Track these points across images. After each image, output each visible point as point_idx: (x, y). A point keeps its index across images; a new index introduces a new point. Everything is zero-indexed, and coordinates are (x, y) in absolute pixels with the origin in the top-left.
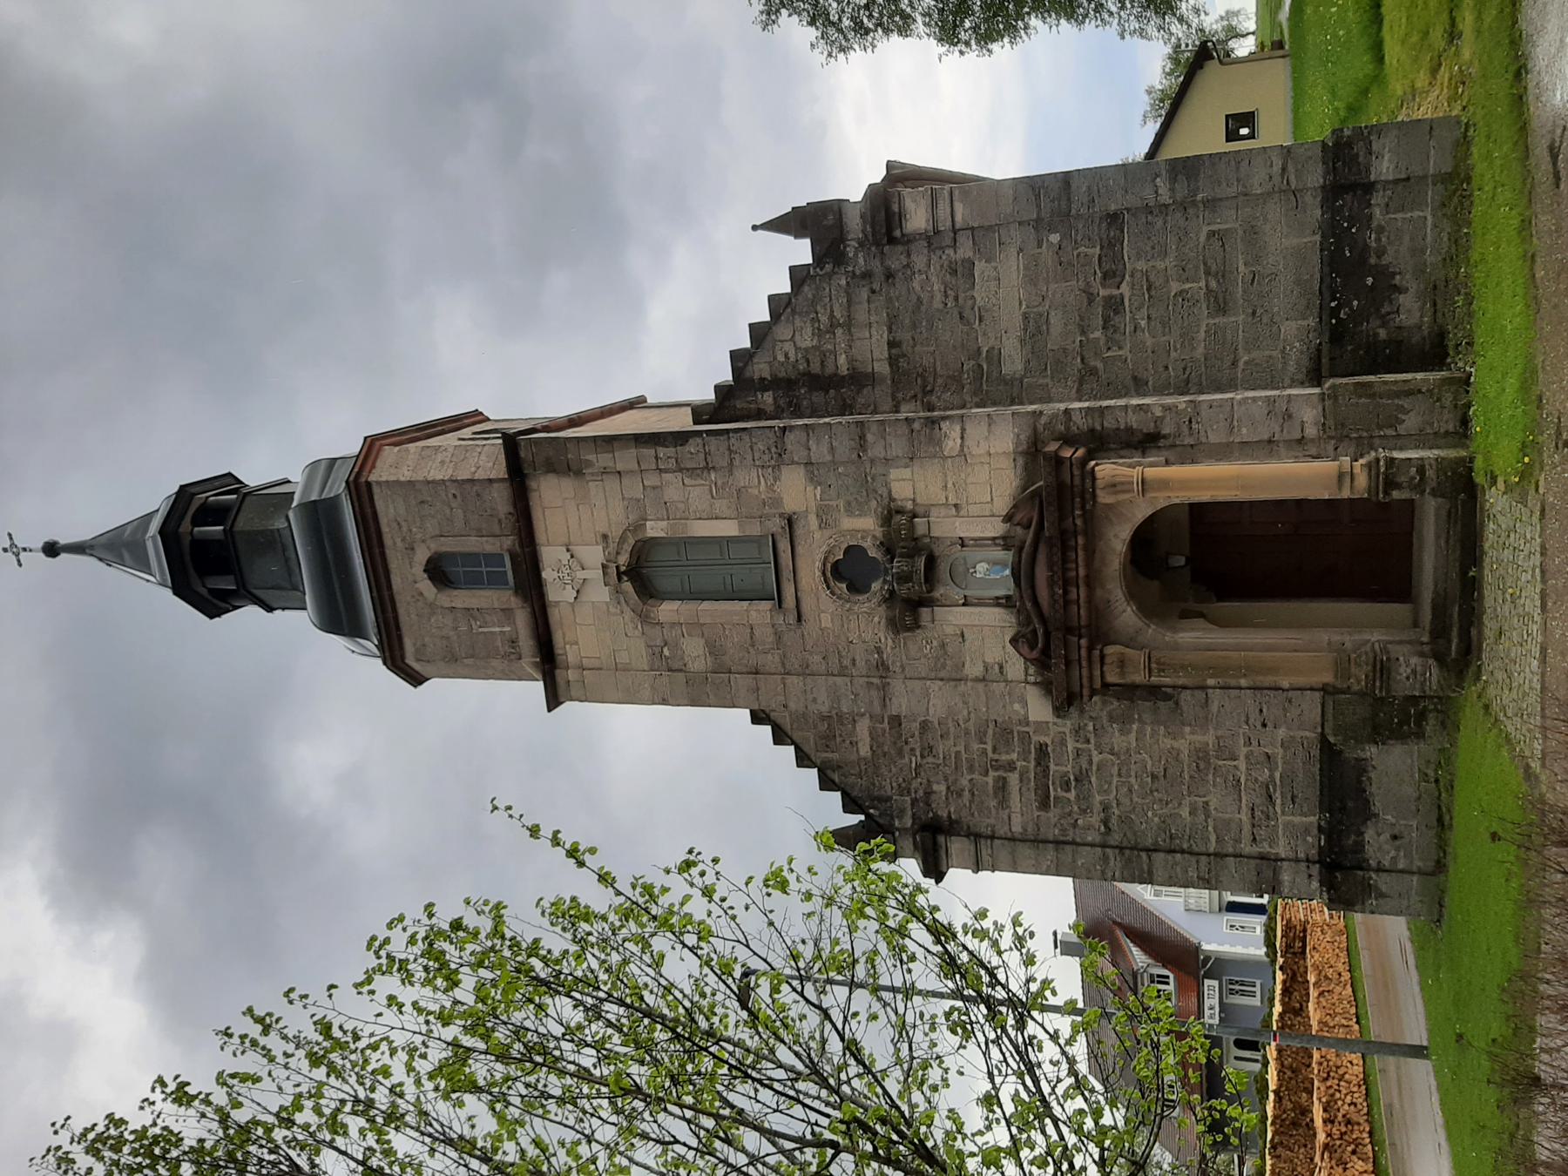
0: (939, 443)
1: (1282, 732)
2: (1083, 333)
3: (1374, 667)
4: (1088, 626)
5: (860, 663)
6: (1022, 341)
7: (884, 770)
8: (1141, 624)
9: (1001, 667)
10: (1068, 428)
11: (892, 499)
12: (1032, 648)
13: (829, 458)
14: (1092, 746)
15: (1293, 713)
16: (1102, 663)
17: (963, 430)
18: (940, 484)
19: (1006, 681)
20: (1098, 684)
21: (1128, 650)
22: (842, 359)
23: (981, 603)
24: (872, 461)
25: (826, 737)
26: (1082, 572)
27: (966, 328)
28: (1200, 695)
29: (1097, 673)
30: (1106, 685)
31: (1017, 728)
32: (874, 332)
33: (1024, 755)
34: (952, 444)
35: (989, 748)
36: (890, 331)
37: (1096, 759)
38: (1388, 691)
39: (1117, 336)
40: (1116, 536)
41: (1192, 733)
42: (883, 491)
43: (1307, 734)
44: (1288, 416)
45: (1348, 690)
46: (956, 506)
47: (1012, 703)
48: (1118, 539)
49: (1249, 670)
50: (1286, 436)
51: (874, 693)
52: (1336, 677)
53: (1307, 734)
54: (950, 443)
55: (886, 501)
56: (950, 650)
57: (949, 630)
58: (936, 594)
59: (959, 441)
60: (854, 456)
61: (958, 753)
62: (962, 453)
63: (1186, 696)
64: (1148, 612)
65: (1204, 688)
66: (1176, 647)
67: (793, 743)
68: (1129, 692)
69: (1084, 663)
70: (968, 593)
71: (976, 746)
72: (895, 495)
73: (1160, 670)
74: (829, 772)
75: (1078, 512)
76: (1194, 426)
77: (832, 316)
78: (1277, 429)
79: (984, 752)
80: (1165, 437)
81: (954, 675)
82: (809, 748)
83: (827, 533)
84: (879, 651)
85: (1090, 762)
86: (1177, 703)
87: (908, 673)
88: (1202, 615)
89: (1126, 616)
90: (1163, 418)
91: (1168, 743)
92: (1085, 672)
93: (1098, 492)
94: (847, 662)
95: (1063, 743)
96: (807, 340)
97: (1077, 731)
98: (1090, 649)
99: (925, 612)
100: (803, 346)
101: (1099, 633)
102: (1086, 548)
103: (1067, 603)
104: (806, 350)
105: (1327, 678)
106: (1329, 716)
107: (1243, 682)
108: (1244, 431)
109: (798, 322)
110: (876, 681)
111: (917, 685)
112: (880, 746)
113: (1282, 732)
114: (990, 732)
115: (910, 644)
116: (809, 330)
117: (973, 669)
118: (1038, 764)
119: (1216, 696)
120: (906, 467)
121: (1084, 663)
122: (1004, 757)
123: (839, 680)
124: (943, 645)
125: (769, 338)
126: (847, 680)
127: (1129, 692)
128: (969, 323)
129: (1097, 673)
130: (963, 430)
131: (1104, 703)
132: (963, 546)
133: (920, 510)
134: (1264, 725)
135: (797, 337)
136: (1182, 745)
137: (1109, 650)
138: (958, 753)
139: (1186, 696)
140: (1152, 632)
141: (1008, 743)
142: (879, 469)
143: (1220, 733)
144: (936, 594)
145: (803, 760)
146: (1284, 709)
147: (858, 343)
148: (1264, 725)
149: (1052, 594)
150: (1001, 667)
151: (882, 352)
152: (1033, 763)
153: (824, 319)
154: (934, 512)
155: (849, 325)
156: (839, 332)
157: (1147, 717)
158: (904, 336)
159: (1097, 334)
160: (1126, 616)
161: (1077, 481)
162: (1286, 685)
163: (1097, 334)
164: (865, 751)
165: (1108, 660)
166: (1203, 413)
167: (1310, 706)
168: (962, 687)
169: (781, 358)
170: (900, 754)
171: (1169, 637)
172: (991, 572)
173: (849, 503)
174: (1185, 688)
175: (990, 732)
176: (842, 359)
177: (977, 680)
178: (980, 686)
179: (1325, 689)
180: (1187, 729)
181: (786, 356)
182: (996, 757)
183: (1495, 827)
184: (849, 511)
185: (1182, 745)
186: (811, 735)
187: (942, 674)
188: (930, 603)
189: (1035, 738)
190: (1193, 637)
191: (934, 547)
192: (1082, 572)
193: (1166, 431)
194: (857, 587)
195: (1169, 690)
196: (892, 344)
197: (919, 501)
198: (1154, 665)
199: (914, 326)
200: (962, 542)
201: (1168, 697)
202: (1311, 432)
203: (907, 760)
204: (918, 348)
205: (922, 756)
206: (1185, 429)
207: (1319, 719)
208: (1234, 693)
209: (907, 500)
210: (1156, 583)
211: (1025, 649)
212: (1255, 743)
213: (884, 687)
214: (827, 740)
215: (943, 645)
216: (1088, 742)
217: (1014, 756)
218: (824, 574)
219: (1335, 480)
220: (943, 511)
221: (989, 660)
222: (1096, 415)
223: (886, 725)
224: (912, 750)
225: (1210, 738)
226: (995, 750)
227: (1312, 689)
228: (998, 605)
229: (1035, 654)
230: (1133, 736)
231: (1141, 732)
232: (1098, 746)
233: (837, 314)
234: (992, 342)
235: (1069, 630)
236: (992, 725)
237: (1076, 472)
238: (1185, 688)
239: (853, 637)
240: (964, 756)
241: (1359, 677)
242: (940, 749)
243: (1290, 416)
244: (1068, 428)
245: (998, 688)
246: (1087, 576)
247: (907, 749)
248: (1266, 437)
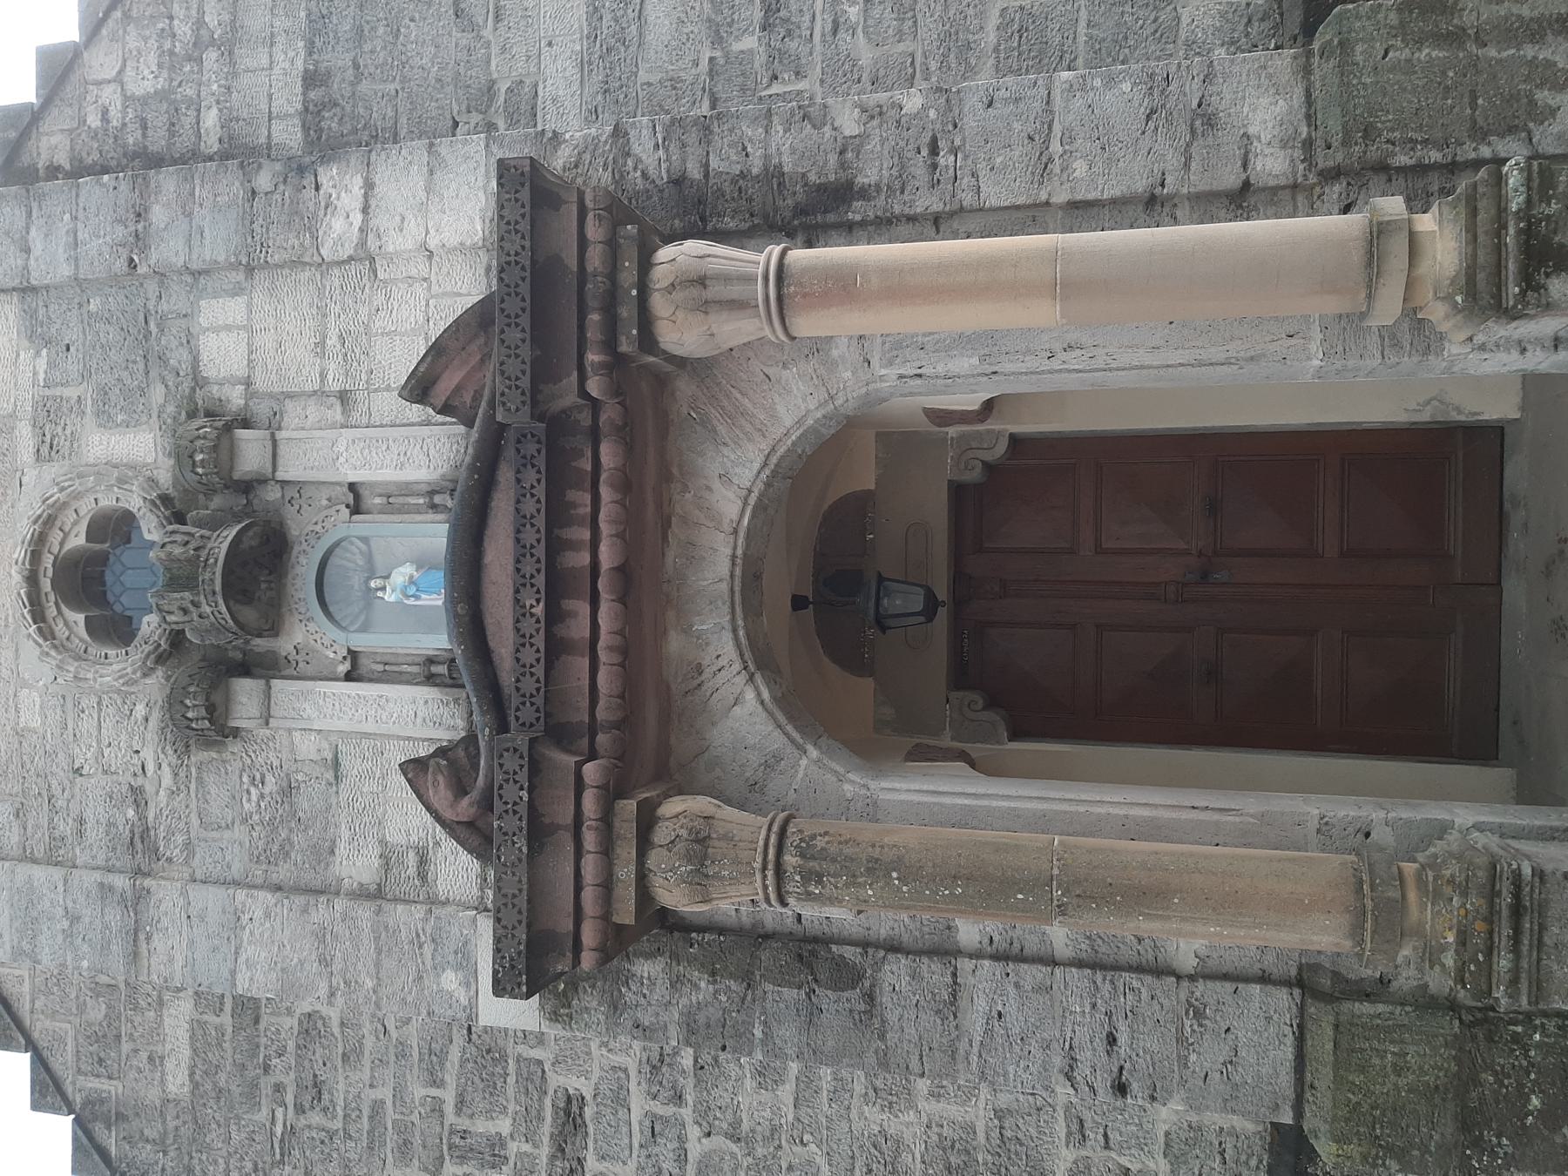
0: (311, 226)
1: (1169, 1114)
2: (718, 40)
3: (1493, 895)
4: (617, 725)
5: (94, 834)
6: (584, 65)
7: (213, 1137)
8: (777, 741)
9: (423, 861)
10: (620, 178)
11: (199, 381)
12: (460, 788)
13: (66, 271)
14: (687, 1113)
15: (1207, 1056)
16: (644, 843)
17: (369, 186)
18: (310, 340)
19: (433, 901)
20: (626, 913)
21: (729, 812)
22: (211, 119)
23: (389, 676)
24: (160, 275)
25: (97, 1038)
26: (607, 556)
27: (465, 39)
28: (934, 973)
29: (625, 873)
30: (667, 922)
31: (515, 1050)
32: (279, 56)
33: (528, 1122)
34: (340, 230)
35: (449, 1096)
36: (310, 49)
37: (695, 1149)
38: (1539, 990)
39: (792, 45)
40: (724, 477)
41: (935, 1095)
42: (179, 358)
43: (1237, 1122)
44: (1205, 119)
45: (1377, 989)
46: (344, 397)
47: (438, 969)
48: (729, 481)
49: (1084, 890)
50: (1199, 181)
51: (114, 916)
52: (1356, 932)
53: (1237, 1122)
54: (338, 225)
55: (186, 386)
56: (303, 803)
57: (308, 747)
58: (284, 646)
59: (357, 219)
60: (120, 265)
61: (377, 1108)
62: (365, 257)
63: (894, 973)
64: (803, 710)
65: (946, 952)
66: (872, 811)
67: (31, 1046)
68: (741, 951)
69: (590, 840)
70: (360, 642)
71: (418, 1091)
72: (209, 371)
73: (810, 876)
74: (99, 1129)
75: (593, 357)
76: (945, 159)
77: (200, 23)
78: (1173, 161)
79: (437, 1109)
80: (864, 194)
81: (308, 877)
82: (63, 1063)
83: (53, 470)
84: (137, 796)
85: (682, 1157)
86: (870, 997)
87: (203, 862)
88: (964, 757)
89: (741, 714)
90: (863, 137)
91: (875, 1117)
92: (590, 866)
93: (660, 305)
94: (65, 827)
95: (620, 1099)
96: (145, 81)
97: (656, 1066)
98: (613, 792)
99: (246, 692)
100: (139, 92)
101: (651, 748)
102: (627, 485)
103: (555, 649)
104: (144, 101)
105: (1324, 937)
106: (1322, 1076)
107: (1060, 936)
108: (1080, 168)
109: (133, 42)
110: (121, 882)
111: (210, 899)
112: (213, 1070)
113: (1169, 1114)
114: (455, 1054)
115: (210, 779)
116: (152, 59)
117: (356, 864)
118: (560, 1150)
119: (981, 978)
120: (237, 291)
121: (590, 840)
122: (481, 1126)
123: (39, 873)
124: (288, 790)
125: (74, 78)
126: (57, 874)
127: (741, 951)
128: (473, 27)
129: (625, 873)
130: (369, 186)
131: (676, 983)
132: (356, 509)
133: (262, 409)
134: (1121, 1089)
135: (129, 72)
136: (907, 1125)
137: (673, 806)
138: (377, 1108)
139: (894, 973)
140: (817, 774)
141: (492, 1088)
142: (176, 300)
143: (1004, 1100)
144: (284, 646)
145: (48, 1091)
146: (1180, 1039)
147: (246, 80)
148: (1121, 1089)
149: (521, 613)
150: (423, 861)
151: (289, 98)
152: (545, 1151)
153: (184, 30)
154: (293, 413)
155: (228, 45)
156: (211, 56)
157: (787, 1033)
158: (338, 59)
159: (749, 42)
160: (741, 714)
161: (596, 258)
162: (1185, 950)
163: (749, 42)
164: (177, 1081)
165: (662, 834)
166: (969, 123)
167: (1260, 1030)
168: (321, 913)
169: (94, 121)
170: (251, 1094)
171: (855, 783)
172: (404, 582)
173: (104, 392)
174: (894, 947)
175: (455, 1054)
176: (211, 119)
177: (363, 894)
178: (364, 913)
179: (1310, 983)
180: (923, 1085)
181: (105, 112)
182: (463, 1123)
183: (1104, 1095)
184: (105, 419)
185: (907, 1125)
186: (66, 1028)
187: (283, 873)
188: (264, 667)
189: (555, 1080)
190: (927, 799)
191: (290, 512)
192: (607, 556)
193: (869, 175)
194: (113, 628)
195: (850, 952)
196: (311, 79)
197: (260, 384)
198: (790, 860)
199: (359, 34)
200: (356, 499)
201: (847, 977)
202: (1272, 165)
203: (263, 1115)
204: (364, 87)
205: (300, 1109)
206: (919, 169)
207: (1286, 1080)
208: (1033, 974)
209: (233, 381)
210: (868, 684)
211: (441, 795)
212: (1096, 1137)
213: (137, 901)
214: (103, 1044)
215: (288, 790)
216: (678, 1098)
217: (504, 1126)
218: (32, 579)
219: (1357, 257)
220: (313, 411)
221: (395, 836)
222: (692, 137)
223: (226, 1019)
224: (279, 1088)
225: (978, 1113)
226: (461, 1103)
227: (1264, 979)
228: (430, 679)
229: (466, 808)
230: (786, 1092)
231: (807, 1083)
232: (704, 1113)
233: (211, 19)
234: (520, 67)
235: (557, 732)
236: (459, 1038)
237: (594, 231)
238: (894, 947)
239: (84, 756)
240: (390, 1115)
241: (1429, 956)
242: (340, 1087)
243: (1210, 122)
244: (620, 178)
245: (405, 917)
246: (623, 571)
247: (266, 1084)
248: (1140, 186)
